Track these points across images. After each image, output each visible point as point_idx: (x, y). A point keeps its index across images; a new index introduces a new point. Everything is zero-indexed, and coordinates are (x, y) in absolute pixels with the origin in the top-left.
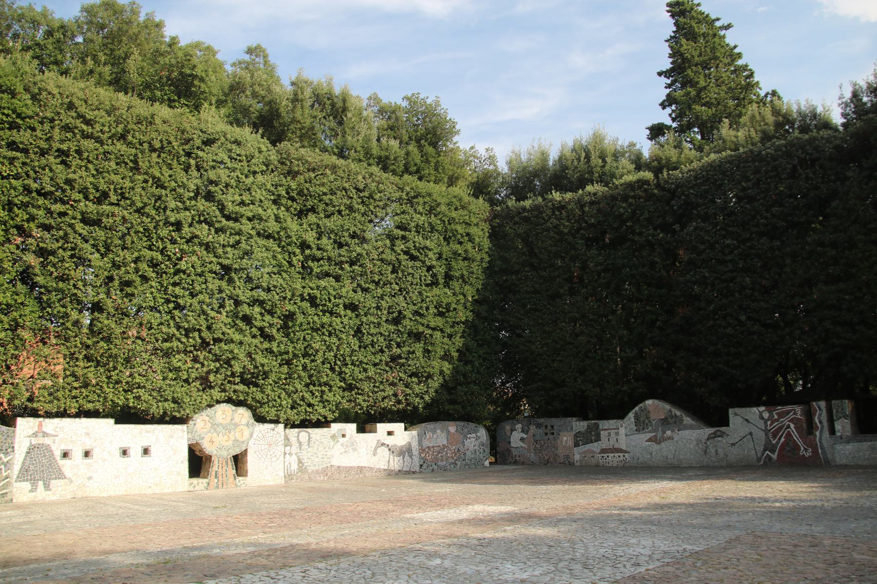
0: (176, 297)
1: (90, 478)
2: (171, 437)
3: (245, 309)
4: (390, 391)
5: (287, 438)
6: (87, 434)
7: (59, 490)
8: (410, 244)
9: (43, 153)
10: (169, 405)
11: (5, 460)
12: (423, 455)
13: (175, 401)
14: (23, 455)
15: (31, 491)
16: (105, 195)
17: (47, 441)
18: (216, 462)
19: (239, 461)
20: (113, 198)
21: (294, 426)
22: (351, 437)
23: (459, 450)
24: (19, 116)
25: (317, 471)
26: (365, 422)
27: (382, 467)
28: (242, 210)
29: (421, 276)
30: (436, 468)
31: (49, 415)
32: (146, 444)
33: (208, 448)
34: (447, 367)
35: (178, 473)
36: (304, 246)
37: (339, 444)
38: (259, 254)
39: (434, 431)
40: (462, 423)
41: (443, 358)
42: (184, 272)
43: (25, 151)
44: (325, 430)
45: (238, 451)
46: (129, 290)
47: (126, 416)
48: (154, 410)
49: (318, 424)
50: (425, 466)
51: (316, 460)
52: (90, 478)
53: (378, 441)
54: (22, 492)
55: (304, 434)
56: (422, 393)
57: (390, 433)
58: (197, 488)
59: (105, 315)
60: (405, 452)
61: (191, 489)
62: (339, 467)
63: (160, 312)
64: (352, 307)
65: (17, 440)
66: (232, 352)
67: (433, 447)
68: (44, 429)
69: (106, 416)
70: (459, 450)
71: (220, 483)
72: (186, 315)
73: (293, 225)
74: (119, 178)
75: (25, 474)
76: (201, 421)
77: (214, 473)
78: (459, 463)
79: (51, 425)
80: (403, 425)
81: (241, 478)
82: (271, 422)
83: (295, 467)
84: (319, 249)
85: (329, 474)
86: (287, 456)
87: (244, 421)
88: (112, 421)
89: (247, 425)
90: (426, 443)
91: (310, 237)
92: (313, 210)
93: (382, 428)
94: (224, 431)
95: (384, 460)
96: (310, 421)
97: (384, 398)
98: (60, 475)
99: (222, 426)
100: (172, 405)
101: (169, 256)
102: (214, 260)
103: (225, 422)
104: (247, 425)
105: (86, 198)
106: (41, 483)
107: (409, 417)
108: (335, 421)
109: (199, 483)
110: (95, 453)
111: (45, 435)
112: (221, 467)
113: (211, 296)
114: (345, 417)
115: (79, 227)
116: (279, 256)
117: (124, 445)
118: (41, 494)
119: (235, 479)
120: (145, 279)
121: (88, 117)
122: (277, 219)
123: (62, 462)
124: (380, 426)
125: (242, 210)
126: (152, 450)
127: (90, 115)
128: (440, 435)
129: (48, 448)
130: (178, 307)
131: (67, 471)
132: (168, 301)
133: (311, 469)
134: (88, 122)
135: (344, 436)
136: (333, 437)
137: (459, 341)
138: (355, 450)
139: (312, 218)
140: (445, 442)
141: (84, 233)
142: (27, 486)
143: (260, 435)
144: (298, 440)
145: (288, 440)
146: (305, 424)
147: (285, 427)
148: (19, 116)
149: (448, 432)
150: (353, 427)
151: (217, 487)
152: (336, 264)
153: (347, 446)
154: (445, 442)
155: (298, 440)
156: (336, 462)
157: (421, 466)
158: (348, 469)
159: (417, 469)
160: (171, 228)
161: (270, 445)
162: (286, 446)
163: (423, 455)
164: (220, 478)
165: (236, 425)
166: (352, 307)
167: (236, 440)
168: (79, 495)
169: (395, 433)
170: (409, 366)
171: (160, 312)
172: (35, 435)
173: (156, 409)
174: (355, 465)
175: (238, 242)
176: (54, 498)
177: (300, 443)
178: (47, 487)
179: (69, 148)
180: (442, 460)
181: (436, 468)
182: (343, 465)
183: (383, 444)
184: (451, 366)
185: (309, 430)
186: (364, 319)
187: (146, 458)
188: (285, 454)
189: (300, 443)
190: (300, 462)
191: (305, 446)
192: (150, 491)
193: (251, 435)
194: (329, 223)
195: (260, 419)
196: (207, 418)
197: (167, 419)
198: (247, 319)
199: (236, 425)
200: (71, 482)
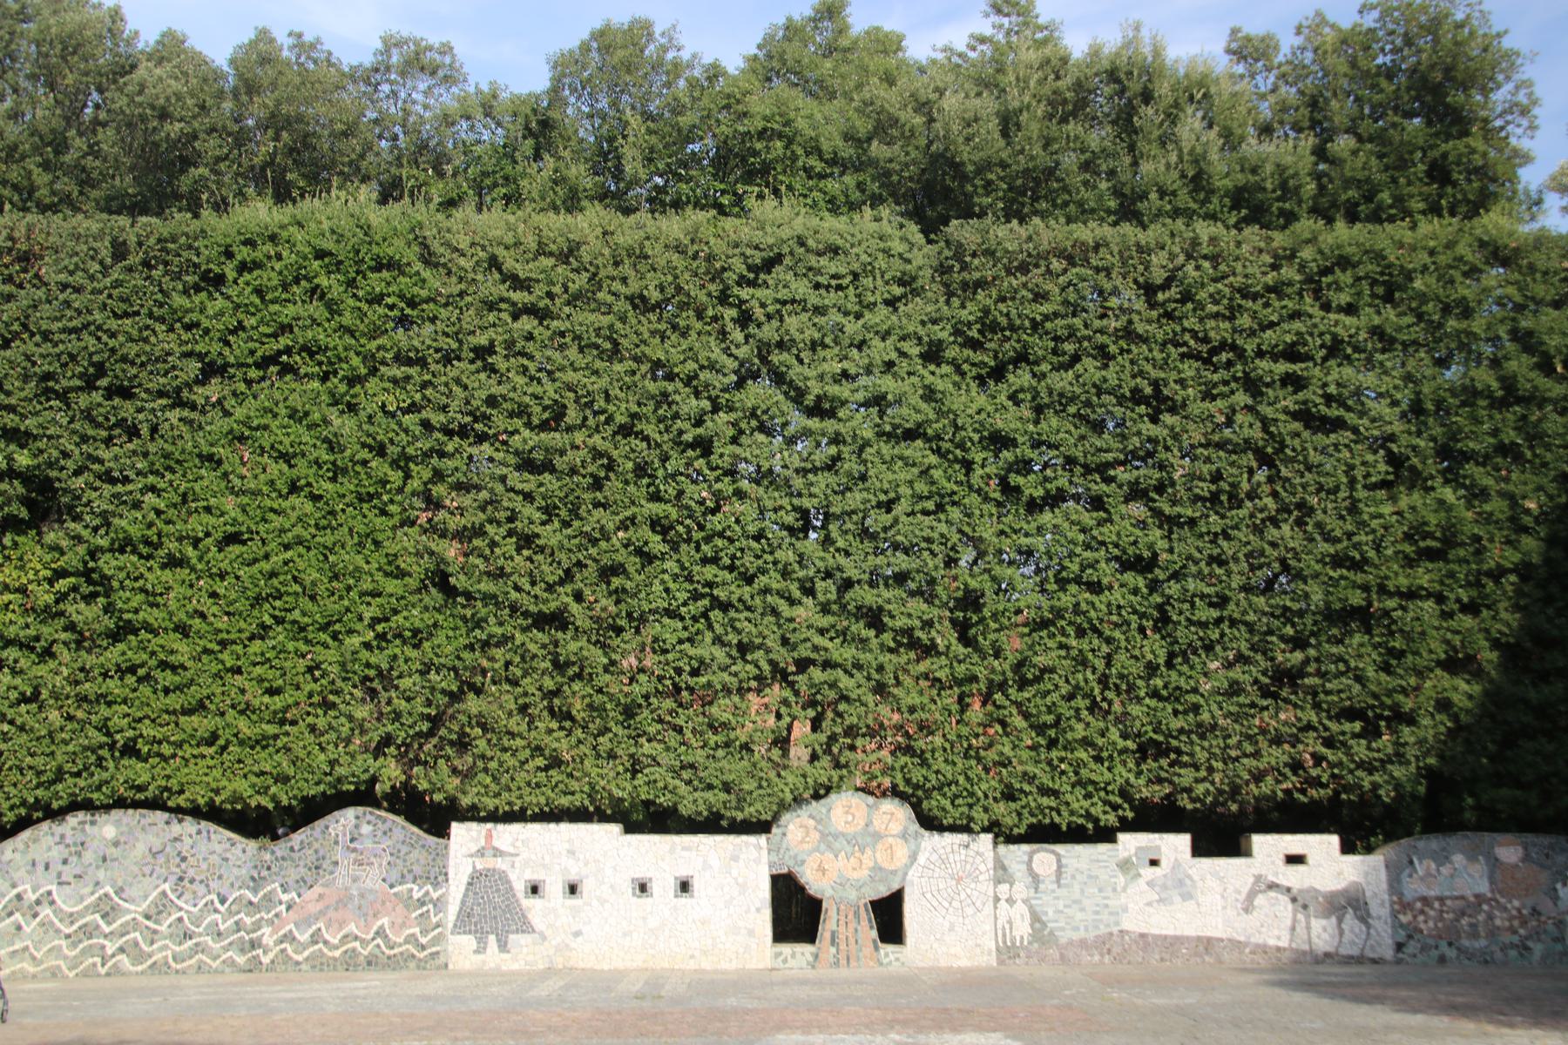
0: (710, 585)
1: (577, 934)
2: (735, 859)
3: (865, 596)
4: (1276, 756)
5: (1000, 866)
6: (571, 852)
7: (523, 955)
8: (1312, 394)
9: (448, 358)
10: (717, 798)
11: (435, 895)
12: (1404, 919)
13: (727, 788)
14: (463, 888)
15: (477, 952)
16: (559, 412)
17: (501, 864)
18: (833, 913)
19: (888, 917)
20: (572, 416)
21: (1012, 839)
22: (1177, 865)
23: (1535, 912)
24: (412, 304)
25: (1083, 943)
26: (1220, 835)
27: (1272, 942)
28: (843, 391)
29: (1352, 467)
30: (1451, 953)
31: (495, 817)
32: (683, 873)
33: (814, 882)
34: (1462, 690)
35: (751, 933)
36: (998, 441)
37: (1142, 882)
38: (881, 477)
39: (1442, 858)
40: (1545, 840)
41: (1452, 665)
42: (721, 535)
43: (422, 362)
44: (1103, 848)
45: (883, 891)
46: (616, 582)
47: (654, 819)
48: (686, 809)
49: (1076, 835)
50: (1412, 947)
51: (1079, 916)
52: (577, 934)
53: (1258, 878)
54: (462, 951)
55: (1044, 857)
56: (1394, 764)
57: (1295, 860)
58: (791, 963)
59: (570, 634)
60: (1348, 904)
61: (779, 963)
62: (1143, 936)
63: (682, 619)
64: (1142, 564)
65: (451, 862)
66: (833, 685)
67: (1441, 899)
68: (496, 843)
69: (603, 818)
70: (1535, 912)
71: (843, 957)
72: (732, 620)
73: (969, 402)
74: (579, 372)
75: (466, 921)
76: (796, 828)
77: (827, 935)
78: (1538, 949)
79: (507, 834)
80: (1334, 840)
81: (890, 948)
82: (953, 829)
83: (1023, 929)
84: (1036, 445)
85: (1116, 950)
86: (1003, 904)
87: (896, 828)
88: (615, 828)
89: (904, 836)
90: (1413, 887)
91: (1010, 420)
92: (1022, 358)
93: (1268, 847)
94: (849, 849)
95: (1274, 926)
96: (1054, 826)
97: (1258, 777)
98: (526, 927)
99: (850, 840)
100: (723, 796)
101: (688, 508)
102: (785, 502)
103: (850, 830)
104: (904, 836)
105: (528, 425)
106: (492, 938)
107: (1358, 826)
108: (1128, 826)
109: (800, 953)
110: (586, 888)
111: (498, 853)
112: (846, 922)
113: (786, 574)
114: (1155, 817)
115: (515, 479)
116: (937, 474)
117: (641, 873)
118: (493, 957)
119: (876, 948)
120: (647, 558)
121: (522, 275)
122: (930, 394)
123: (529, 903)
124: (1259, 841)
125: (843, 391)
126: (696, 885)
127: (522, 271)
128: (1458, 872)
129: (503, 877)
130: (718, 604)
131: (536, 919)
132: (696, 596)
133: (1064, 936)
134: (518, 283)
135: (1154, 863)
136: (1125, 865)
137: (1507, 620)
138: (1187, 897)
139: (1021, 378)
140: (1484, 887)
141: (527, 487)
142: (469, 941)
143: (934, 857)
144: (1030, 869)
145: (1004, 868)
146: (1043, 834)
147: (996, 843)
148: (412, 304)
149: (1494, 863)
150: (1183, 841)
151: (837, 964)
152: (1088, 470)
153: (1165, 887)
154: (1484, 887)
155: (1030, 869)
156: (1133, 923)
157: (1399, 947)
158: (1171, 944)
159: (1389, 953)
160: (690, 453)
161: (959, 880)
162: (998, 881)
163: (1404, 919)
164: (843, 946)
165: (878, 837)
166: (1142, 564)
167: (877, 868)
168: (559, 963)
169: (1310, 860)
170: (1327, 693)
171: (682, 619)
172: (481, 853)
173: (691, 803)
174: (1190, 931)
175: (837, 459)
176: (515, 967)
177: (1036, 879)
178: (503, 946)
179: (492, 342)
180: (1474, 935)
181: (1451, 953)
182: (1156, 931)
183: (1272, 886)
184: (1476, 689)
185: (1060, 849)
186: (1173, 589)
187: (684, 900)
188: (997, 899)
189: (1036, 879)
190: (1036, 918)
191: (1048, 885)
192: (692, 965)
193: (913, 857)
194: (1062, 381)
195: (929, 822)
196: (812, 822)
197: (724, 823)
198: (874, 617)
199: (878, 837)
200: (544, 938)
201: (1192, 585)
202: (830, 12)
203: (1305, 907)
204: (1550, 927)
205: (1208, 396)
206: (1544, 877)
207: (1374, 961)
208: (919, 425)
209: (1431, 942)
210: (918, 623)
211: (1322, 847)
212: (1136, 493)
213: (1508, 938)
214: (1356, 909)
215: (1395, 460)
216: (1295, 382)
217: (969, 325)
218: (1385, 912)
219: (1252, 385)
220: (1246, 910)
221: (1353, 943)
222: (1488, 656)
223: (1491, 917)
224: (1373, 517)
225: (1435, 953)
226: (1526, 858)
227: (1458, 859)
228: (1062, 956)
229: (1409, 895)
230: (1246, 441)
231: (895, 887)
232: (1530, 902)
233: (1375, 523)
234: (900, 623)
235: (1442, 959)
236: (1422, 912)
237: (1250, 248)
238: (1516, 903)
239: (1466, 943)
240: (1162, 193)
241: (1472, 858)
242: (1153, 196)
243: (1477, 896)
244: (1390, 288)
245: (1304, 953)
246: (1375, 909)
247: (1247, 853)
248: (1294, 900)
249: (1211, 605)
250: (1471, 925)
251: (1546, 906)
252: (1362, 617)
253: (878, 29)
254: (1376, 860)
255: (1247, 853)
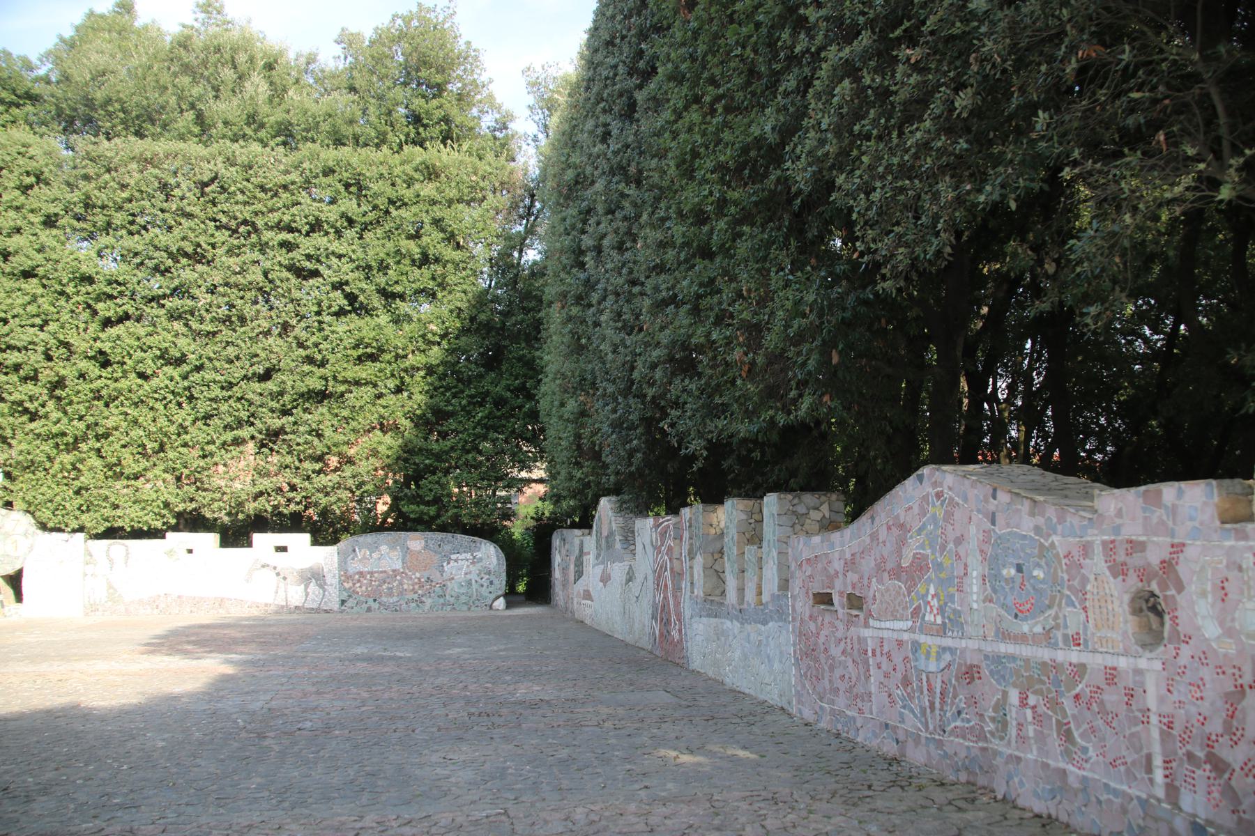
26: (236, 534)
30: (375, 606)
39: (374, 548)
50: (351, 603)
55: (117, 547)
60: (314, 576)
67: (372, 573)
78: (428, 602)
90: (354, 566)
93: (263, 541)
107: (326, 529)
108: (175, 528)
114: (193, 522)
124: (257, 537)
140: (398, 566)
146: (112, 533)
154: (398, 566)
157: (343, 602)
159: (336, 607)
180: (390, 595)
201: (208, 375)
202: (126, 8)
203: (285, 578)
204: (437, 589)
205: (230, 252)
206: (436, 558)
207: (327, 611)
208: (34, 269)
209: (363, 599)
210: (26, 398)
211: (299, 541)
212: (174, 316)
213: (411, 596)
214: (317, 580)
215: (351, 298)
216: (287, 246)
217: (75, 204)
218: (335, 581)
219: (263, 247)
220: (247, 581)
221: (313, 600)
222: (406, 423)
223: (401, 584)
224: (333, 332)
225: (365, 606)
226: (426, 547)
227: (384, 548)
228: (127, 610)
229: (351, 571)
230: (251, 283)
231: (18, 567)
232: (426, 574)
233: (332, 337)
234: (16, 396)
235: (369, 610)
236: (359, 581)
237: (273, 162)
238: (418, 575)
239: (384, 599)
240: (226, 123)
241: (393, 548)
242: (220, 125)
243: (394, 571)
244: (356, 186)
245: (282, 607)
246: (329, 580)
247: (250, 545)
248: (278, 574)
249: (222, 388)
250: (389, 589)
251: (436, 577)
252: (321, 396)
253: (468, 57)
254: (331, 550)
255: (250, 545)
